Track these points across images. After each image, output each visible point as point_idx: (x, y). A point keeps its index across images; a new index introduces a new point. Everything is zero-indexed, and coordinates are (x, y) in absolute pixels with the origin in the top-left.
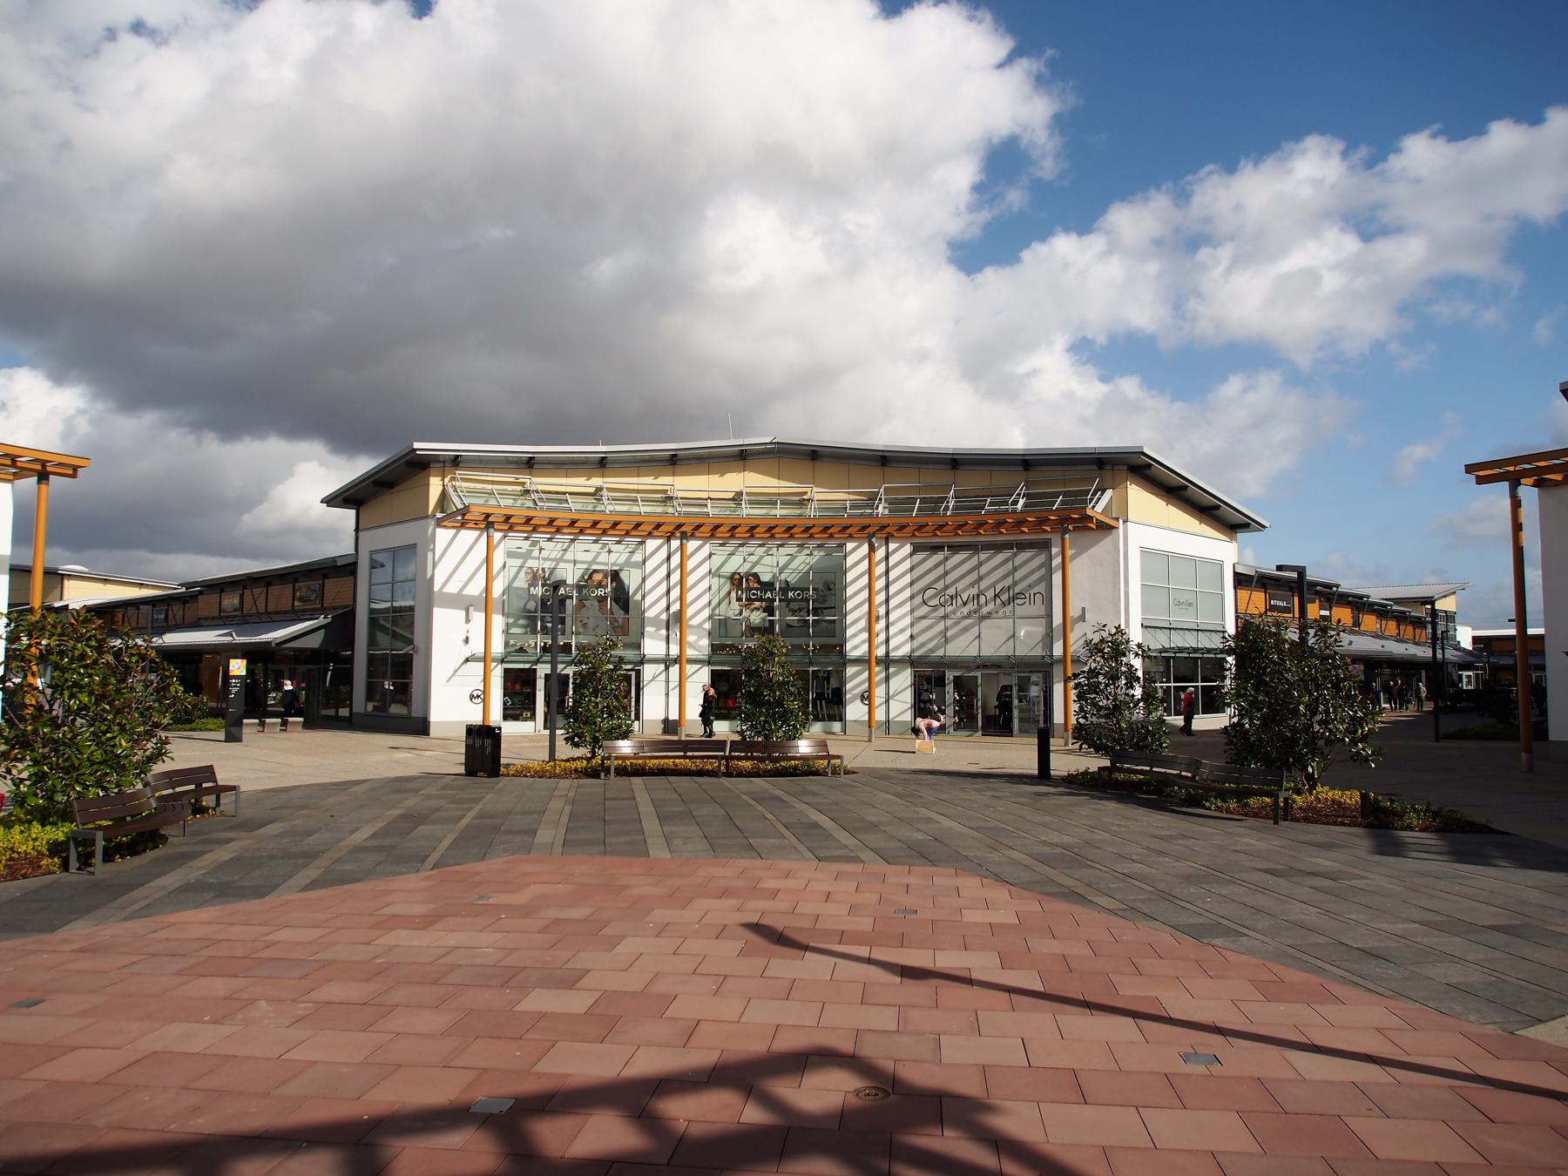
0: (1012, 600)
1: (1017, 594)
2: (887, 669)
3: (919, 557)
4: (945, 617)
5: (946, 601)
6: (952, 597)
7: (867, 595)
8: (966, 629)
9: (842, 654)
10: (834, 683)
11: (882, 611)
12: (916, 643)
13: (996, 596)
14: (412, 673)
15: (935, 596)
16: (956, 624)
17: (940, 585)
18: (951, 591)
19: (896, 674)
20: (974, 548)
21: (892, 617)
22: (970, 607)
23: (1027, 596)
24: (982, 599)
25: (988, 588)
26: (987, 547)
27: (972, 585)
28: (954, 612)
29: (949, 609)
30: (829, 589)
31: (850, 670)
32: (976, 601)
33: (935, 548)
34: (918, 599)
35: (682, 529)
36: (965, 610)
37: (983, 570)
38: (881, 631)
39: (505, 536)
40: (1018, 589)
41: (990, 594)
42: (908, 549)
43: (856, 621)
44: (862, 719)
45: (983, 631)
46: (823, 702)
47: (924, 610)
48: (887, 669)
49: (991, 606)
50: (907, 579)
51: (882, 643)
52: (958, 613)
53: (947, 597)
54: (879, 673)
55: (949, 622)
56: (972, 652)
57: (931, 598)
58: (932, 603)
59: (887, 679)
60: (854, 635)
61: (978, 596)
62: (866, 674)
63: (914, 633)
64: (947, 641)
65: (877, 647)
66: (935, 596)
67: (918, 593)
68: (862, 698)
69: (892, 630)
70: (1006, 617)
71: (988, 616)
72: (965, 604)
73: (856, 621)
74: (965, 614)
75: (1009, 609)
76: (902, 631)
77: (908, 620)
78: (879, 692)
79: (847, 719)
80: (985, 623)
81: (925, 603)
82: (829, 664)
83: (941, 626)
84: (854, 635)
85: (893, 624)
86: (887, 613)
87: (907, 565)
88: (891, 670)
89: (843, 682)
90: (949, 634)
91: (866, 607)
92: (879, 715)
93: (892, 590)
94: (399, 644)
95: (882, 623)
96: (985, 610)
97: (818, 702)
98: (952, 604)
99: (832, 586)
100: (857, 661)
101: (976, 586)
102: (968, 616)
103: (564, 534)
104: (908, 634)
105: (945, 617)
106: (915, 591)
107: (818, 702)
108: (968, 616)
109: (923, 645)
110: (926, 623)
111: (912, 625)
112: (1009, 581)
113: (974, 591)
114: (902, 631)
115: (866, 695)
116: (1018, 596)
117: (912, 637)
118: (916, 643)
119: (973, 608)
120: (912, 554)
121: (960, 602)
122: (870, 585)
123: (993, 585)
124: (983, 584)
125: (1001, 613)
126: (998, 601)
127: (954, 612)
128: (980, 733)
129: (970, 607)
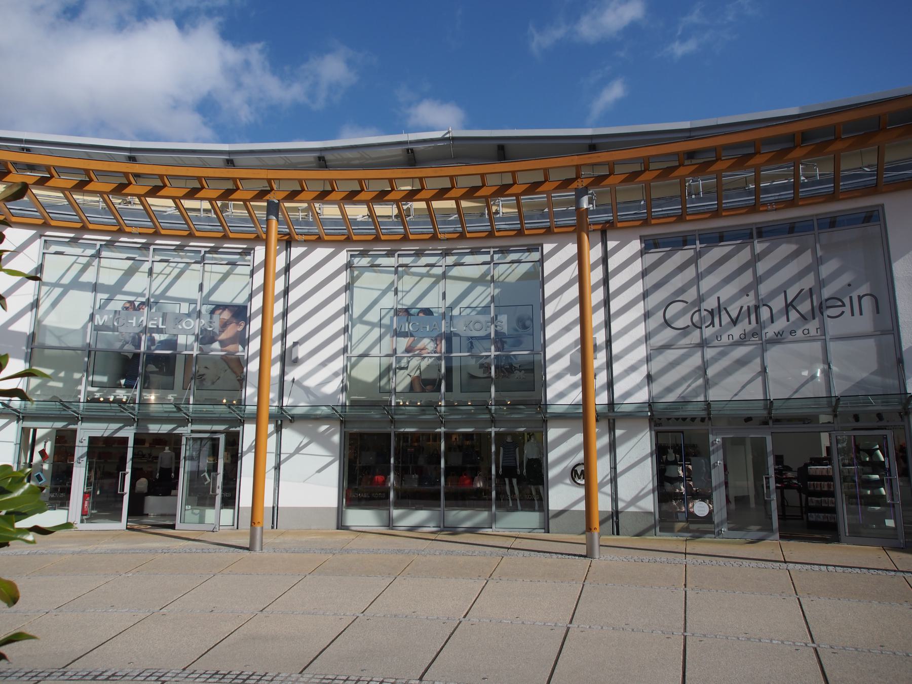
0: (819, 310)
1: (827, 300)
2: (612, 429)
3: (651, 258)
4: (703, 344)
5: (702, 320)
6: (711, 313)
7: (576, 273)
8: (741, 363)
9: (541, 405)
10: (530, 452)
11: (600, 337)
12: (657, 388)
13: (789, 306)
14: (8, 274)
15: (683, 312)
16: (723, 354)
17: (691, 295)
18: (711, 303)
19: (626, 438)
20: (747, 235)
21: (616, 347)
22: (744, 326)
23: (847, 301)
24: (765, 313)
25: (773, 294)
26: (762, 232)
27: (745, 291)
28: (717, 336)
29: (708, 332)
30: (525, 327)
31: (553, 433)
32: (753, 317)
33: (683, 241)
34: (657, 320)
35: (268, 197)
36: (736, 332)
37: (762, 267)
38: (600, 369)
39: (41, 236)
40: (826, 293)
41: (778, 303)
42: (635, 245)
43: (558, 356)
44: (576, 508)
45: (768, 362)
46: (515, 481)
47: (667, 334)
48: (612, 429)
49: (781, 324)
50: (638, 288)
51: (602, 387)
52: (725, 339)
53: (704, 313)
54: (599, 436)
55: (710, 353)
56: (755, 392)
57: (678, 316)
58: (680, 323)
59: (612, 447)
60: (559, 376)
61: (757, 308)
62: (579, 438)
63: (652, 373)
64: (707, 385)
65: (596, 394)
66: (683, 312)
67: (656, 309)
68: (574, 474)
69: (617, 368)
70: (812, 339)
71: (778, 339)
72: (735, 322)
73: (558, 356)
74: (736, 337)
75: (813, 326)
76: (633, 369)
77: (641, 352)
78: (601, 468)
79: (550, 508)
80: (773, 353)
81: (667, 323)
82: (519, 422)
83: (696, 360)
84: (559, 376)
85: (620, 357)
86: (609, 342)
87: (637, 267)
88: (618, 432)
89: (543, 448)
90: (711, 372)
91: (576, 332)
92: (603, 504)
93: (614, 284)
94: (6, 402)
95: (602, 357)
96: (770, 331)
97: (507, 480)
98: (712, 323)
99: (528, 323)
100: (562, 417)
101: (752, 294)
102: (742, 341)
103: (130, 234)
104: (643, 370)
105: (703, 344)
106: (649, 285)
107: (507, 480)
108: (742, 341)
109: (669, 390)
110: (671, 355)
111: (648, 359)
112: (808, 282)
113: (749, 301)
114: (633, 369)
115: (579, 469)
116: (830, 303)
117: (650, 378)
118: (657, 388)
119: (749, 328)
120: (643, 253)
121: (725, 319)
122: (581, 278)
123: (783, 289)
124: (764, 289)
125: (799, 333)
126: (793, 315)
127: (717, 336)
128: (777, 535)
129: (744, 326)
